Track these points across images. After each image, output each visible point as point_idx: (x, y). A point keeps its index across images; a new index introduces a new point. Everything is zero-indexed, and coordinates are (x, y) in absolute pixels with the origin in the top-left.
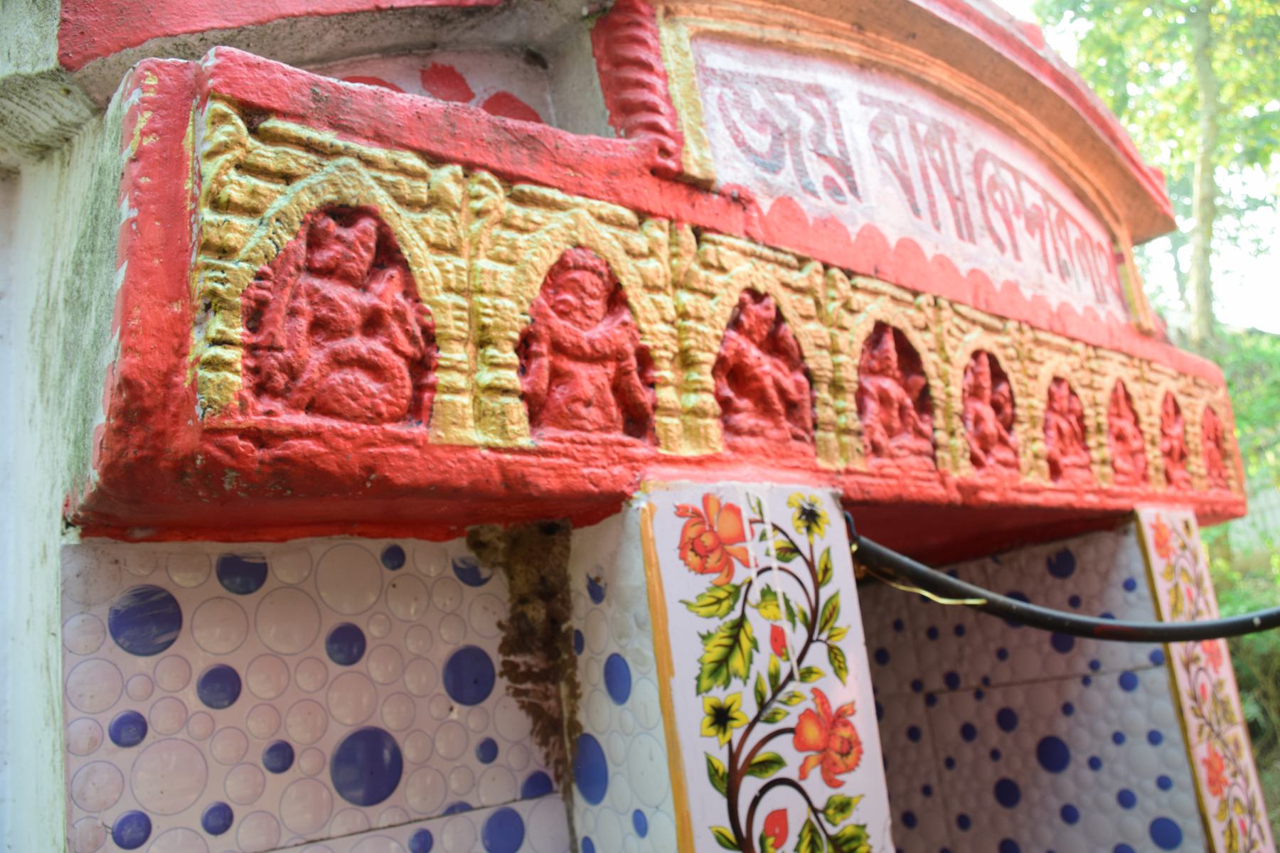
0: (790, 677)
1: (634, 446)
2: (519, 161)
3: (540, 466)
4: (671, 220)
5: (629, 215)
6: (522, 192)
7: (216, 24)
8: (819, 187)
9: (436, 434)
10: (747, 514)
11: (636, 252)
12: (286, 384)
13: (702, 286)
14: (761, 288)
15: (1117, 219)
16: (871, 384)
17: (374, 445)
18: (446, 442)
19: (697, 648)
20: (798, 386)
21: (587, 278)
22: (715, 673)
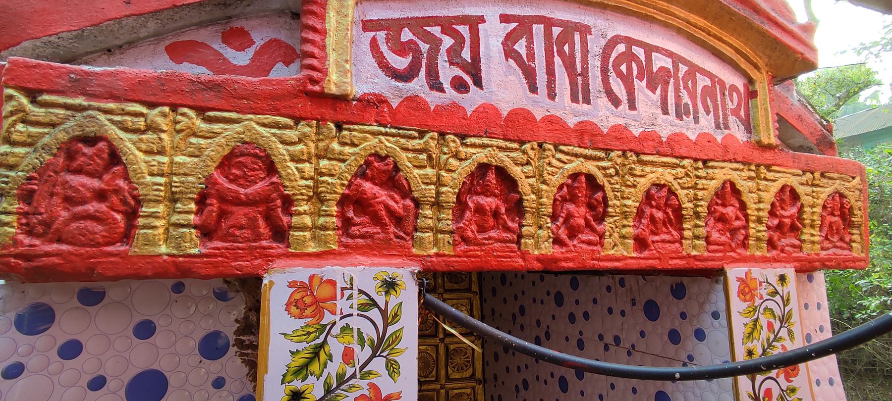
0: (354, 376)
1: (272, 248)
2: (207, 99)
4: (318, 120)
6: (209, 116)
8: (447, 86)
9: (136, 249)
13: (337, 156)
14: (383, 153)
15: (756, 67)
16: (648, 211)
19: (288, 358)
20: (405, 208)
22: (748, 337)
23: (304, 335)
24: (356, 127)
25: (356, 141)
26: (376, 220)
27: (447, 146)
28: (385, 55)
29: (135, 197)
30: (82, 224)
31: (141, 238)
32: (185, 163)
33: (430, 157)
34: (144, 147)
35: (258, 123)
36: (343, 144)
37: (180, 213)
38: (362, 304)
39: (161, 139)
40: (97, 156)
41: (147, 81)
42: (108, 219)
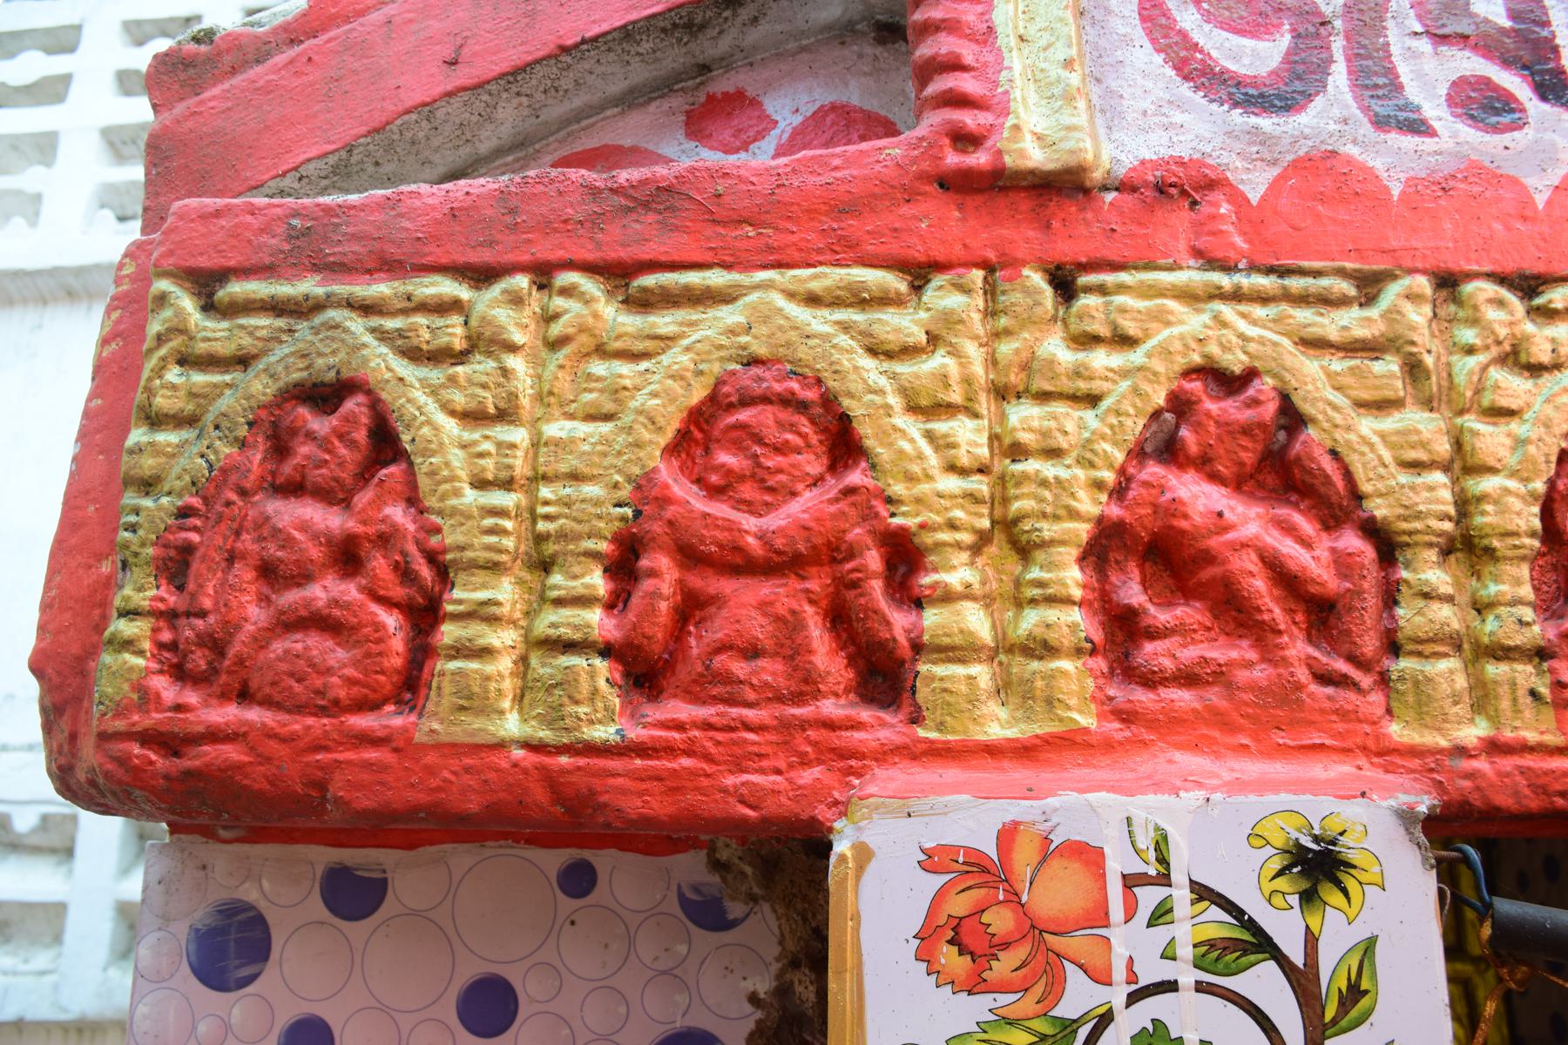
1: (858, 725)
2: (619, 242)
3: (628, 774)
5: (895, 282)
6: (645, 290)
7: (314, 152)
8: (1434, 110)
9: (435, 723)
10: (1118, 863)
11: (894, 347)
12: (209, 663)
13: (1066, 385)
14: (1235, 362)
17: (326, 749)
18: (445, 739)
20: (1343, 564)
21: (761, 417)
24: (1124, 277)
25: (1131, 328)
26: (1233, 611)
27: (1474, 322)
28: (1196, 36)
29: (433, 557)
30: (297, 643)
31: (448, 688)
32: (572, 441)
33: (1413, 369)
34: (459, 399)
35: (791, 295)
36: (1087, 341)
37: (559, 602)
38: (1211, 944)
39: (505, 372)
40: (341, 437)
41: (475, 207)
42: (360, 625)
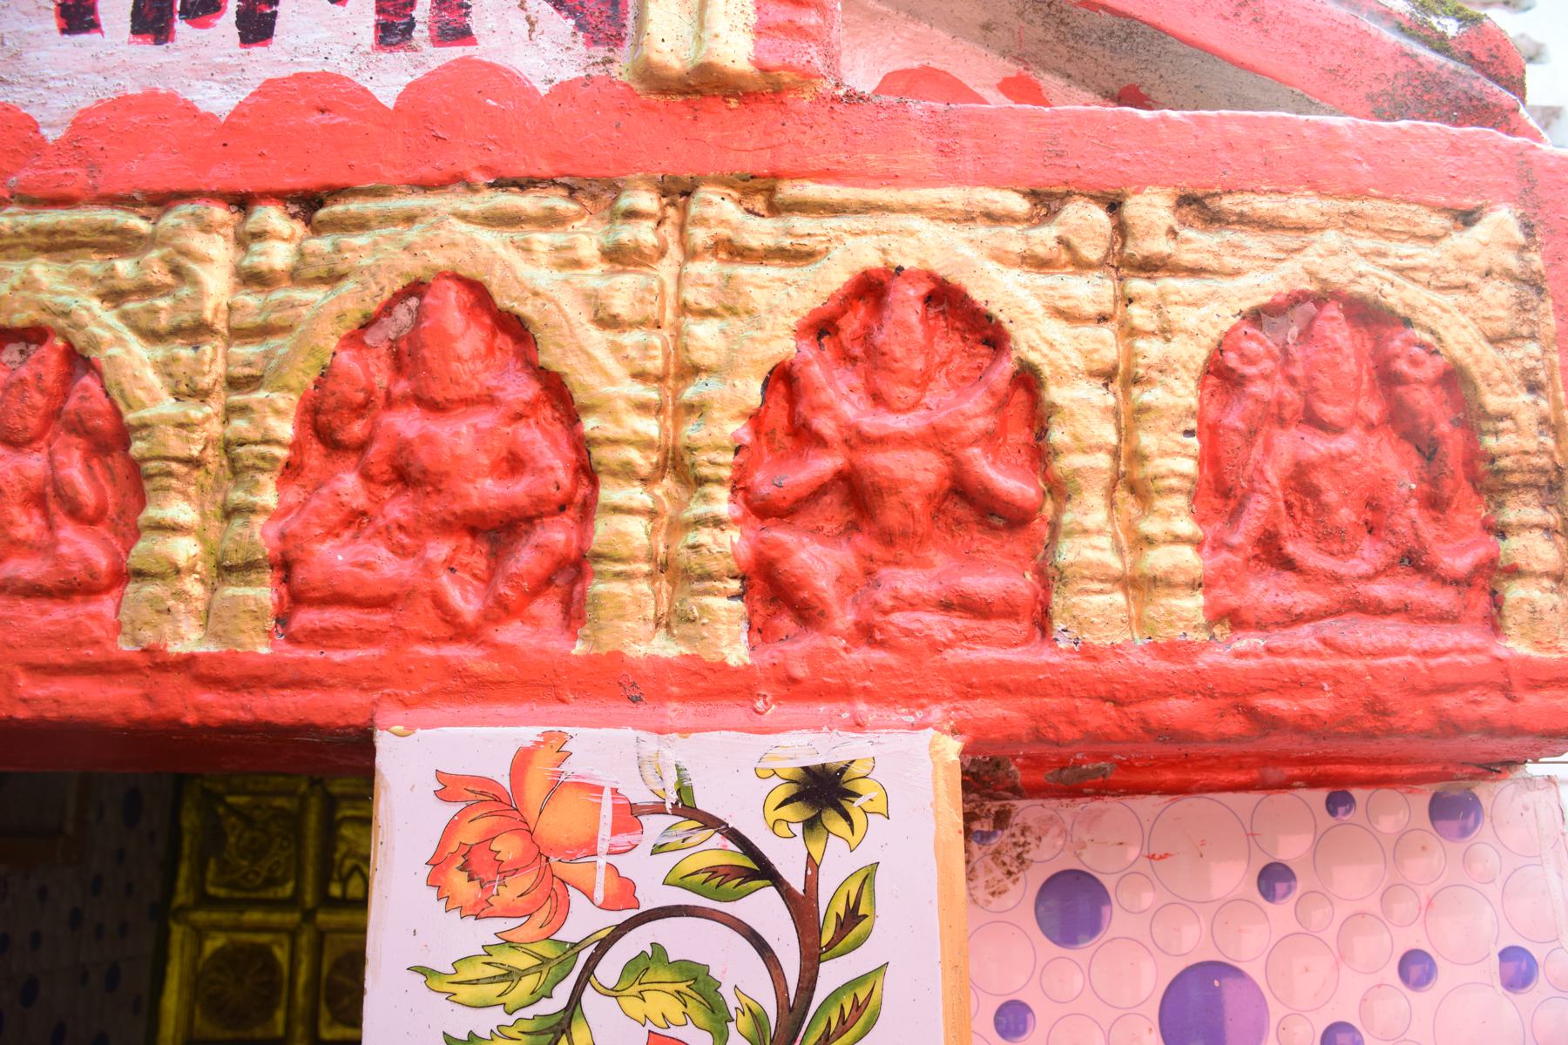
23: (492, 980)
24: (910, 196)
